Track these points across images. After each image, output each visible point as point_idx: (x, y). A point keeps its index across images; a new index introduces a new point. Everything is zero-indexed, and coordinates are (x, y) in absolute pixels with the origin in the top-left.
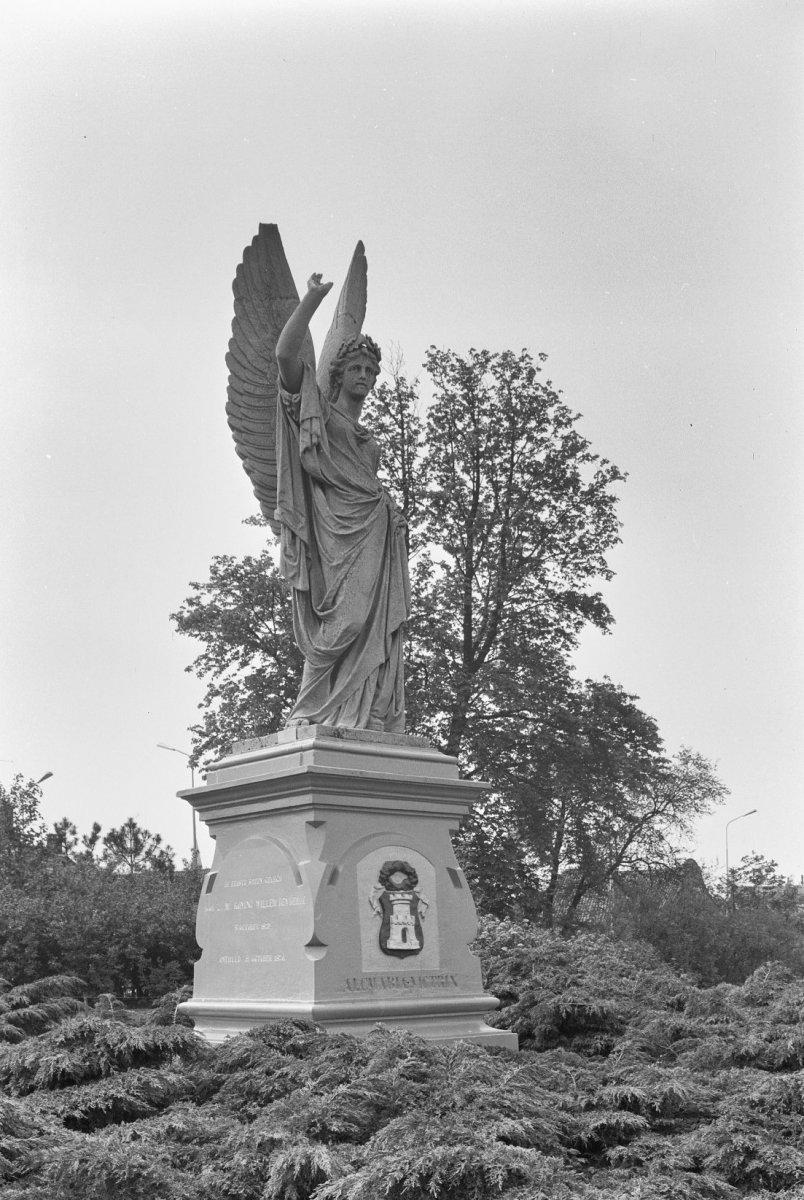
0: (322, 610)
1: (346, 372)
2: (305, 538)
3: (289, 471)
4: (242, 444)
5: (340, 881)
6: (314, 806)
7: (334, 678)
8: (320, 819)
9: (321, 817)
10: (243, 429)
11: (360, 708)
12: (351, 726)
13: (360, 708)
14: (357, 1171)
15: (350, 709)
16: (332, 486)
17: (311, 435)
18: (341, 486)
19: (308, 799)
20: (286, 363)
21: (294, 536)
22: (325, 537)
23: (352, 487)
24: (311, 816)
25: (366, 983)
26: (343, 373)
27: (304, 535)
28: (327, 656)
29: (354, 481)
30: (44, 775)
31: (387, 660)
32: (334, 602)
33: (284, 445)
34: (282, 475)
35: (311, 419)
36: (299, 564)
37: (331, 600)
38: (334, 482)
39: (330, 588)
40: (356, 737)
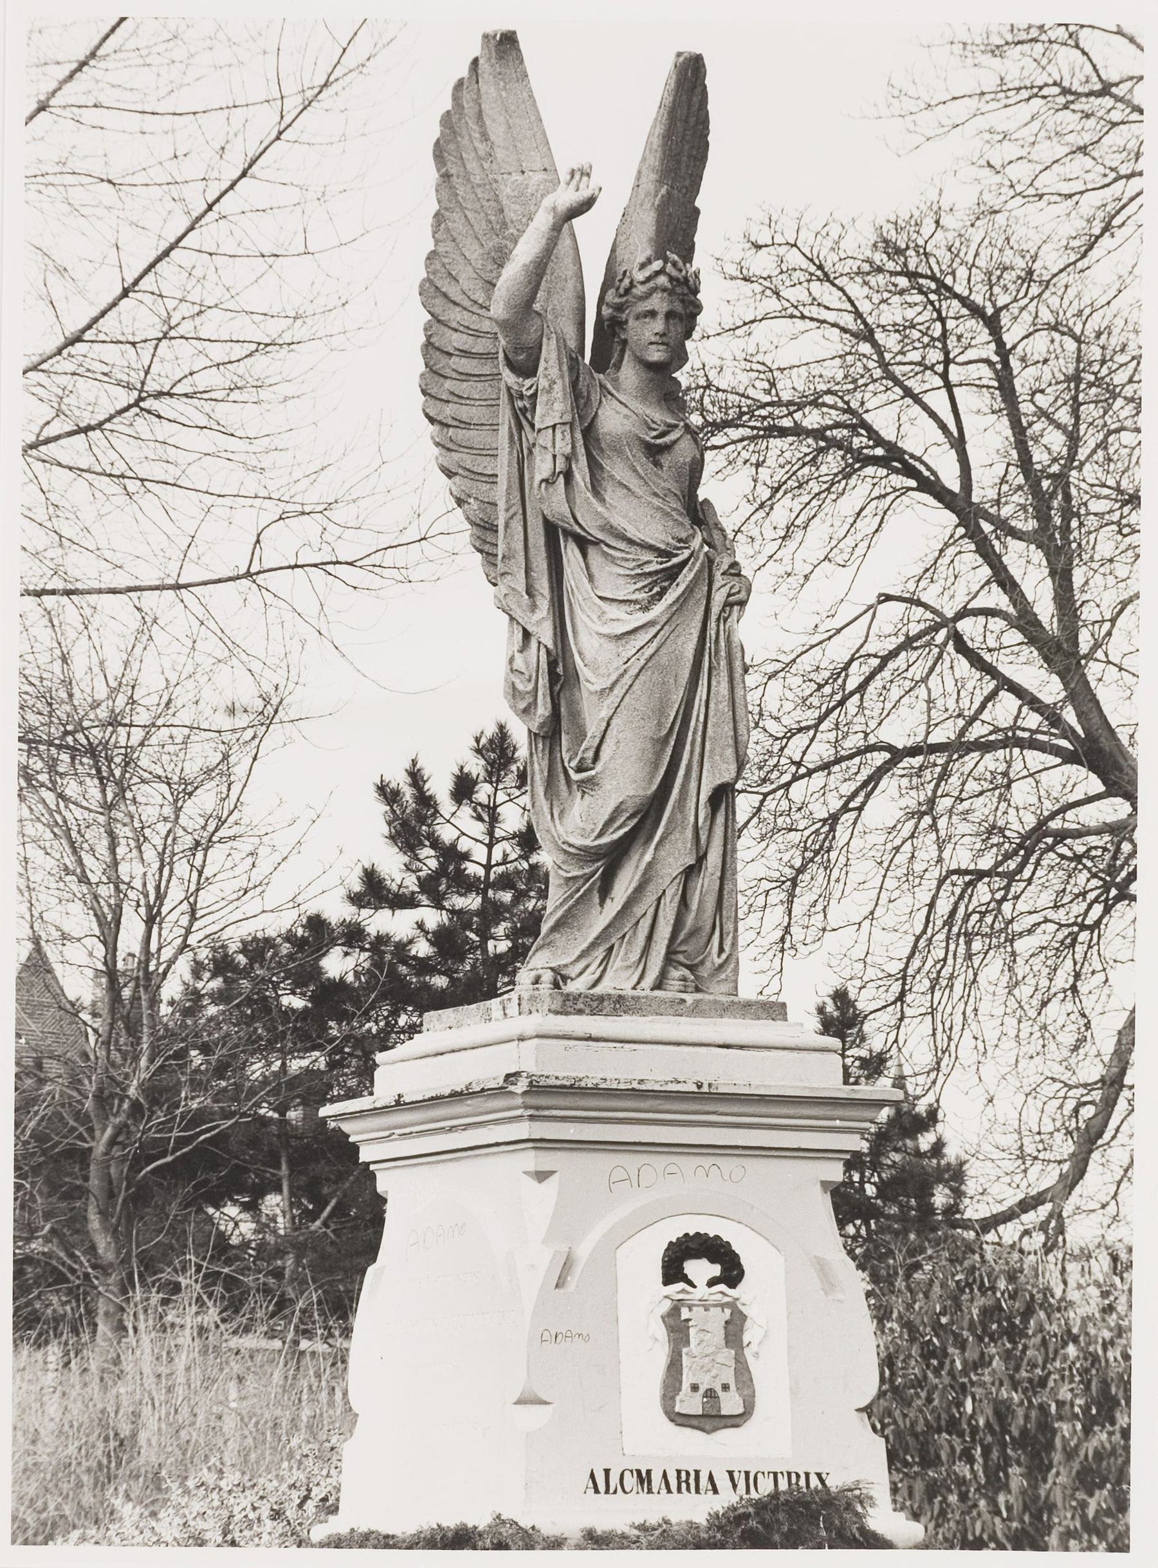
0: (579, 770)
1: (631, 322)
2: (547, 639)
3: (519, 517)
4: (449, 450)
5: (573, 1281)
6: (540, 1144)
7: (605, 890)
8: (546, 1168)
9: (546, 1160)
10: (450, 422)
11: (646, 951)
12: (627, 990)
13: (646, 951)
14: (237, 1311)
15: (626, 955)
16: (597, 543)
17: (554, 456)
18: (613, 543)
19: (523, 1130)
20: (509, 326)
21: (527, 635)
22: (583, 637)
23: (631, 542)
24: (531, 1160)
25: (630, 1481)
26: (626, 322)
27: (545, 634)
28: (586, 855)
29: (632, 533)
30: (451, 1522)
31: (701, 858)
32: (596, 757)
33: (564, 389)
34: (507, 526)
35: (554, 427)
36: (536, 689)
37: (590, 754)
38: (600, 536)
39: (593, 729)
40: (619, 1004)
